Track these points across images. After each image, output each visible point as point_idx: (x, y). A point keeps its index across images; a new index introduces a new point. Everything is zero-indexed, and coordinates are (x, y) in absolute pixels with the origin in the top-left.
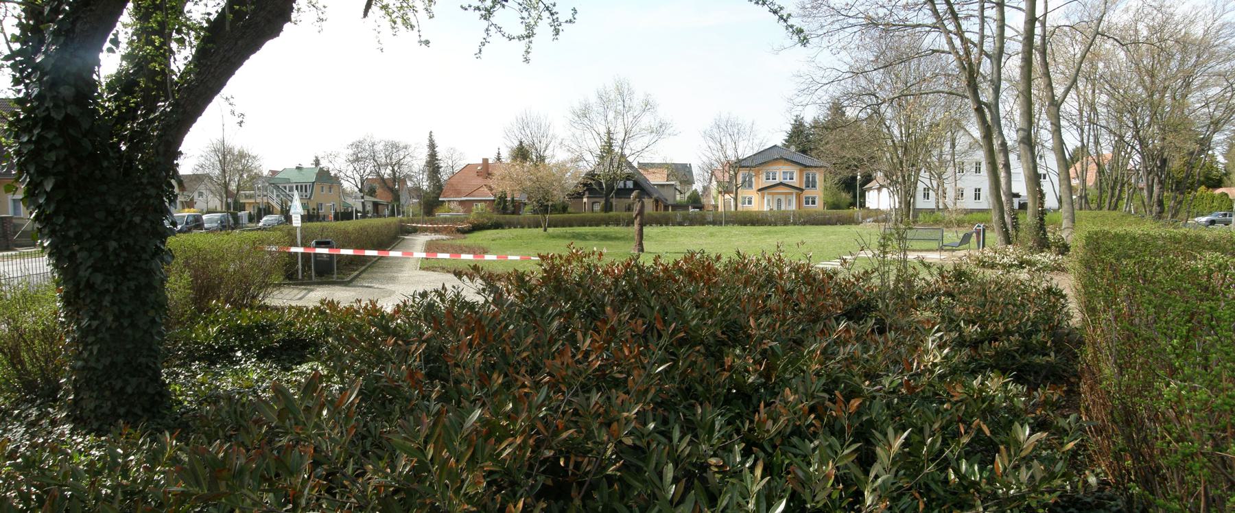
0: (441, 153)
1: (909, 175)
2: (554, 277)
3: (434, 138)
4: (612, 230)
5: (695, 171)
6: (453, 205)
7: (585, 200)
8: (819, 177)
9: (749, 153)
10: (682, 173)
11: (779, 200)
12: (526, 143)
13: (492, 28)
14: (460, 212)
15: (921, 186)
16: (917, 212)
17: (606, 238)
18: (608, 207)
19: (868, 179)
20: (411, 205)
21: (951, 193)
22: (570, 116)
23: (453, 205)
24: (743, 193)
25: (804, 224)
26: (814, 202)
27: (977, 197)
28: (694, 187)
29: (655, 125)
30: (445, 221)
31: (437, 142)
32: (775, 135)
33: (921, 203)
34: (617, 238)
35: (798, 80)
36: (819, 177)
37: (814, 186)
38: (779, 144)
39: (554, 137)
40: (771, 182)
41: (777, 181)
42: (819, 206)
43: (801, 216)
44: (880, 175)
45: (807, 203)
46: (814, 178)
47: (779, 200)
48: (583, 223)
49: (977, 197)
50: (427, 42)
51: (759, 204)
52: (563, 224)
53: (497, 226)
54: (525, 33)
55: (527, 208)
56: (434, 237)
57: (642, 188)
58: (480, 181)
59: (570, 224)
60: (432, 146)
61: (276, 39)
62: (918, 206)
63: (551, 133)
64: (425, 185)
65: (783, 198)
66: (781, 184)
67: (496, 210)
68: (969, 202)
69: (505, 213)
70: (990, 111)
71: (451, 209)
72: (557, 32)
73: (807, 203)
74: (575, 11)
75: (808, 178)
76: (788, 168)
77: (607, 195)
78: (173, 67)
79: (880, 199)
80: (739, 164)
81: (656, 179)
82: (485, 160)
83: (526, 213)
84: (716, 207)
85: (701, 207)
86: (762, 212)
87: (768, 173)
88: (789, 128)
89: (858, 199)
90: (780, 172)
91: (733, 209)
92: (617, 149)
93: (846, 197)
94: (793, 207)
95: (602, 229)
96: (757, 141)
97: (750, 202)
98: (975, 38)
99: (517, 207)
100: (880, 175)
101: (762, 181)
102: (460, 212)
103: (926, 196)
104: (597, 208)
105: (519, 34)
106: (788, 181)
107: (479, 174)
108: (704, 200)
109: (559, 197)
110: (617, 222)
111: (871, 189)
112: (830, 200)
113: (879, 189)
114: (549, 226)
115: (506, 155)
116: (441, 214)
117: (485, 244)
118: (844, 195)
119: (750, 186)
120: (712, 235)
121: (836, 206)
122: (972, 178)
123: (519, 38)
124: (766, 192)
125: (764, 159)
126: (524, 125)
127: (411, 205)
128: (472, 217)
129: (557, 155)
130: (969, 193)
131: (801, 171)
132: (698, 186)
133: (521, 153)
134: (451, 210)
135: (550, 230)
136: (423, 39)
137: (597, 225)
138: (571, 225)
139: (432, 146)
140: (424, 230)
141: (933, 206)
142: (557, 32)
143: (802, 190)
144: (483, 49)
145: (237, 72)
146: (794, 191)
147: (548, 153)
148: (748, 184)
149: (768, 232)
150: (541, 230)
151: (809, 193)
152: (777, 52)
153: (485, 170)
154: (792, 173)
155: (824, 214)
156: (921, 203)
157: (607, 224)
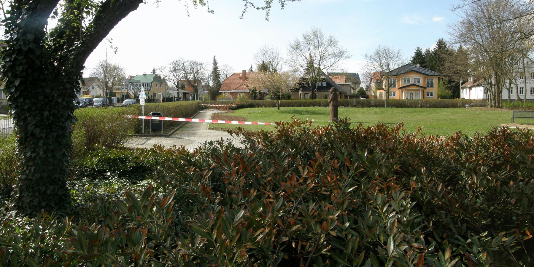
0: (220, 67)
3: (216, 59)
4: (316, 109)
5: (361, 77)
6: (226, 95)
7: (300, 92)
8: (435, 81)
10: (354, 78)
11: (412, 94)
12: (266, 62)
14: (231, 98)
17: (313, 113)
18: (313, 97)
20: (204, 94)
22: (290, 48)
23: (226, 95)
24: (392, 90)
26: (432, 95)
28: (361, 86)
29: (337, 52)
30: (222, 103)
32: (408, 57)
37: (432, 86)
39: (281, 59)
40: (407, 84)
41: (410, 83)
42: (435, 97)
45: (428, 95)
46: (432, 82)
47: (412, 94)
48: (300, 105)
50: (212, 12)
51: (399, 95)
53: (251, 106)
54: (265, 6)
55: (268, 96)
56: (216, 111)
58: (241, 82)
60: (215, 63)
63: (280, 57)
64: (211, 84)
65: (414, 92)
66: (413, 85)
71: (225, 97)
73: (428, 95)
75: (428, 82)
81: (339, 81)
83: (268, 99)
85: (367, 97)
88: (413, 55)
89: (456, 93)
90: (412, 78)
94: (420, 97)
95: (311, 108)
96: (400, 62)
99: (262, 96)
101: (401, 84)
104: (307, 96)
106: (417, 83)
107: (241, 78)
108: (368, 93)
110: (319, 105)
111: (465, 88)
113: (470, 88)
116: (220, 99)
119: (395, 86)
121: (443, 97)
123: (262, 8)
124: (404, 89)
125: (403, 71)
126: (265, 53)
127: (204, 94)
128: (238, 101)
129: (283, 68)
131: (424, 77)
132: (363, 85)
133: (264, 67)
134: (225, 97)
135: (281, 109)
136: (210, 10)
138: (293, 106)
139: (215, 63)
140: (211, 108)
143: (426, 88)
146: (421, 89)
149: (415, 112)
150: (276, 108)
151: (429, 90)
153: (244, 76)
154: (419, 79)
157: (314, 106)
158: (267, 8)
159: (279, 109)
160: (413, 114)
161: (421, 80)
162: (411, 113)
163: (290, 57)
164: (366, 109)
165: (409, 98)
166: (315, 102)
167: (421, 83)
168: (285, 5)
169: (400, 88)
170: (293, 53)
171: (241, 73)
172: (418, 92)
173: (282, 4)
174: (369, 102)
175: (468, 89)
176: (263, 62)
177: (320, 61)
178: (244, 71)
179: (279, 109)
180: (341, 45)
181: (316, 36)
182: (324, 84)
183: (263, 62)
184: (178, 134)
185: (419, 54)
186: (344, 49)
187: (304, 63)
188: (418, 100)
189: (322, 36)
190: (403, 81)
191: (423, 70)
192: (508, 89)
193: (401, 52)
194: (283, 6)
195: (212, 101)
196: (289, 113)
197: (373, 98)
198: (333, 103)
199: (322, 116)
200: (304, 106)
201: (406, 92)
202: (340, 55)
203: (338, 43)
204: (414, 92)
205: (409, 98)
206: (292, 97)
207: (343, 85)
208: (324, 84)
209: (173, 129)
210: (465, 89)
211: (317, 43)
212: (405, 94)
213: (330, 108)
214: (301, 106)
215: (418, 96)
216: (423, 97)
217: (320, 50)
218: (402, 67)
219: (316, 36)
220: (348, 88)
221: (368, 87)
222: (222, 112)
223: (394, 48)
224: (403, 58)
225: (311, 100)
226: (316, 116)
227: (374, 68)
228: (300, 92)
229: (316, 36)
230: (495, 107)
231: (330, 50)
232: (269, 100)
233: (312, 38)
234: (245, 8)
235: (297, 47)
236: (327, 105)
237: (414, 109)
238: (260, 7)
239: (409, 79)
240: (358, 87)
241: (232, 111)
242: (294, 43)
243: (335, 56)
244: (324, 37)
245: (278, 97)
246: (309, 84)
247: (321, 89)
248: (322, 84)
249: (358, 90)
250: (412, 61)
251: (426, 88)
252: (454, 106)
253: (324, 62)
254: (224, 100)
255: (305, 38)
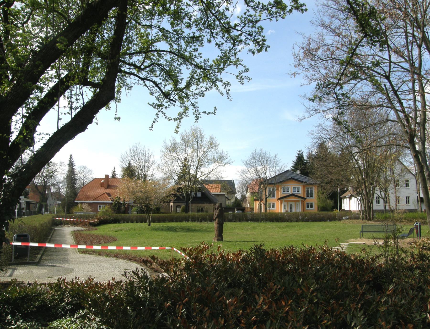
0: (77, 168)
1: (370, 190)
2: (197, 264)
3: (74, 159)
4: (190, 224)
5: (237, 186)
6: (84, 206)
7: (172, 204)
8: (315, 191)
9: (273, 175)
10: (229, 186)
11: (291, 206)
12: (133, 164)
13: (160, 113)
14: (89, 211)
15: (375, 195)
16: (374, 211)
17: (189, 230)
18: (186, 210)
19: (343, 192)
20: (54, 205)
21: (392, 199)
22: (164, 150)
23: (84, 206)
24: (271, 200)
25: (308, 221)
26: (312, 207)
27: (408, 202)
28: (236, 195)
29: (216, 156)
30: (80, 217)
31: (75, 163)
32: (287, 163)
33: (376, 207)
34: (195, 231)
35: (312, 136)
36: (315, 191)
37: (312, 196)
38: (290, 169)
39: (153, 162)
40: (286, 194)
41: (290, 193)
42: (314, 209)
43: (306, 215)
44: (350, 188)
45: (308, 207)
46: (312, 191)
47: (291, 206)
48: (172, 220)
49: (408, 202)
50: (119, 119)
51: (279, 208)
52: (159, 220)
53: (116, 221)
54: (178, 117)
55: (134, 209)
56: (77, 228)
57: (206, 197)
58: (103, 190)
59: (163, 220)
60: (71, 164)
61: (83, 133)
62: (374, 208)
63: (151, 160)
64: (64, 191)
65: (293, 204)
66: (292, 195)
67: (113, 209)
68: (403, 206)
69: (119, 213)
70: (421, 155)
71: (83, 209)
72: (197, 118)
73: (308, 207)
74: (215, 108)
75: (308, 191)
76: (296, 185)
77: (187, 202)
78: (10, 139)
79: (351, 204)
80: (265, 182)
81: (214, 190)
82: (107, 176)
83: (134, 213)
84: (252, 209)
85: (243, 209)
86: (282, 214)
87: (284, 188)
88: (295, 159)
89: (337, 205)
90: (291, 187)
91: (263, 211)
92: (192, 172)
93: (330, 203)
94: (300, 210)
95: (184, 224)
96: (278, 168)
97: (273, 207)
98: (412, 115)
99: (127, 208)
100: (350, 188)
101: (280, 193)
102: (89, 211)
103: (378, 202)
104: (179, 210)
105: (174, 117)
106: (296, 193)
107: (102, 185)
108: (244, 205)
109: (154, 204)
110: (194, 219)
111: (345, 197)
112: (321, 205)
113: (350, 198)
114: (154, 222)
115: (119, 174)
116: (77, 212)
117: (112, 234)
118: (329, 201)
119: (274, 196)
120: (254, 228)
121: (323, 209)
122: (404, 190)
123: (174, 119)
124: (283, 200)
125: (283, 179)
126: (135, 154)
127: (54, 205)
128: (99, 215)
129: (156, 173)
130: (403, 201)
131: (304, 187)
132: (238, 196)
133: (130, 172)
134: (82, 209)
135: (152, 224)
136: (117, 117)
137: (181, 221)
138: (164, 221)
139: (71, 164)
140: (67, 223)
141: (382, 208)
142: (197, 118)
143: (305, 199)
144: (154, 125)
145: (61, 150)
146: (300, 199)
147: (149, 173)
148: (272, 194)
149: (288, 227)
150: (145, 225)
151: (309, 200)
152: (301, 120)
153: (107, 183)
154: (298, 188)
155: (318, 214)
156: (376, 207)
157: (187, 221)
158: (179, 119)
159: (149, 225)
160: (285, 230)
161: (301, 190)
162: (283, 228)
163: (164, 162)
164: (244, 224)
165: (289, 211)
166: (189, 216)
167: (301, 194)
168: (200, 118)
169: (279, 199)
170: (168, 156)
171: (102, 179)
172: (297, 203)
173: (196, 116)
174: (246, 216)
175: (348, 199)
176: (130, 164)
177: (197, 167)
178: (107, 176)
179: (149, 225)
180: (223, 147)
181: (195, 137)
182: (199, 195)
183: (130, 164)
184: (46, 260)
185: (300, 158)
186: (225, 154)
187: (177, 167)
188: (296, 213)
189: (202, 137)
190: (282, 190)
191: (303, 178)
192: (383, 199)
193: (278, 157)
194: (198, 119)
195: (68, 215)
196: (162, 230)
197: (249, 210)
198: (219, 221)
199: (199, 234)
200: (177, 221)
201: (286, 203)
202: (221, 159)
203: (219, 147)
204: (293, 204)
205: (289, 211)
206: (162, 210)
207: (218, 195)
208: (199, 195)
209: (38, 254)
210: (345, 199)
211: (196, 146)
212: (285, 206)
213: (214, 225)
214: (173, 221)
215: (297, 208)
216: (303, 209)
217: (199, 154)
218: (279, 175)
219: (196, 137)
220: (224, 199)
221: (244, 197)
222: (83, 229)
223: (270, 151)
224: (280, 164)
225: (184, 214)
226: (192, 233)
227: (251, 175)
228: (172, 204)
229: (196, 137)
230: (366, 219)
231: (210, 155)
232: (135, 214)
233: (190, 139)
234: (156, 117)
235: (173, 148)
236: (211, 220)
237: (288, 224)
238: (172, 117)
239: (288, 188)
240: (232, 197)
241: (93, 227)
242: (170, 144)
243: (215, 162)
244: (205, 139)
245: (148, 210)
246: (183, 194)
247: (196, 200)
248: (196, 194)
249: (233, 200)
250: (293, 166)
251: (305, 199)
252: (332, 219)
253: (202, 169)
254: (82, 213)
255: (183, 139)
